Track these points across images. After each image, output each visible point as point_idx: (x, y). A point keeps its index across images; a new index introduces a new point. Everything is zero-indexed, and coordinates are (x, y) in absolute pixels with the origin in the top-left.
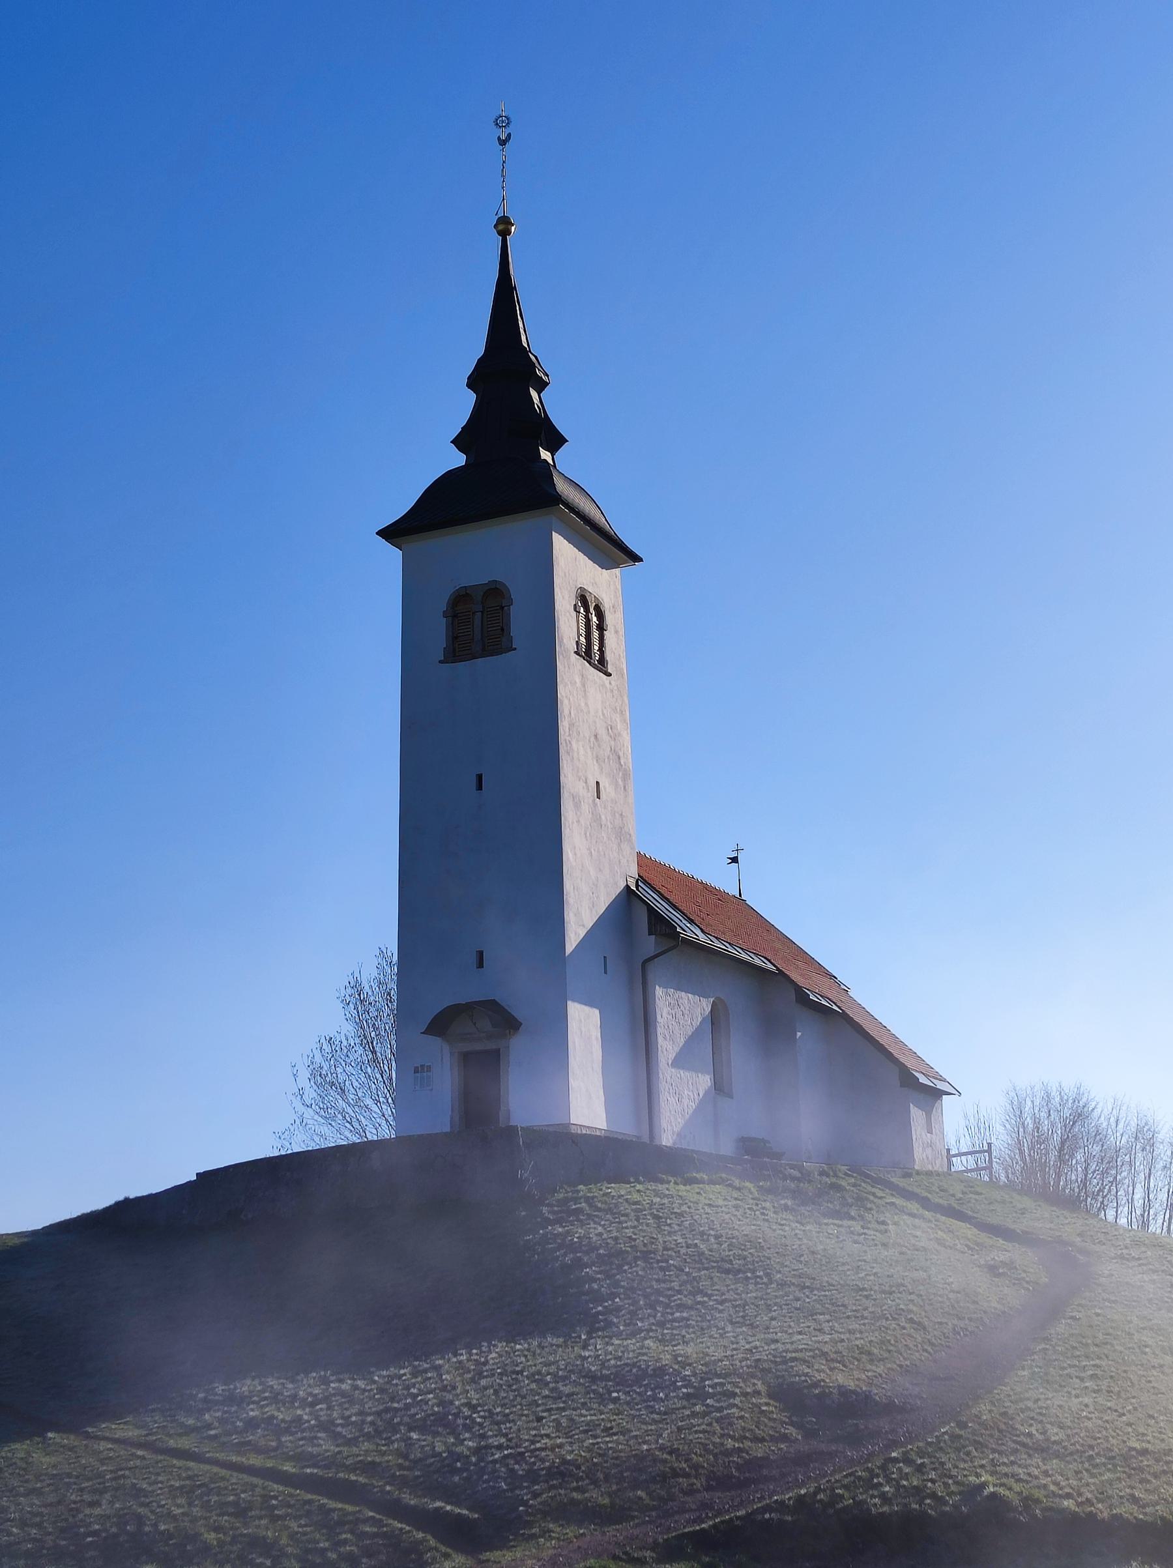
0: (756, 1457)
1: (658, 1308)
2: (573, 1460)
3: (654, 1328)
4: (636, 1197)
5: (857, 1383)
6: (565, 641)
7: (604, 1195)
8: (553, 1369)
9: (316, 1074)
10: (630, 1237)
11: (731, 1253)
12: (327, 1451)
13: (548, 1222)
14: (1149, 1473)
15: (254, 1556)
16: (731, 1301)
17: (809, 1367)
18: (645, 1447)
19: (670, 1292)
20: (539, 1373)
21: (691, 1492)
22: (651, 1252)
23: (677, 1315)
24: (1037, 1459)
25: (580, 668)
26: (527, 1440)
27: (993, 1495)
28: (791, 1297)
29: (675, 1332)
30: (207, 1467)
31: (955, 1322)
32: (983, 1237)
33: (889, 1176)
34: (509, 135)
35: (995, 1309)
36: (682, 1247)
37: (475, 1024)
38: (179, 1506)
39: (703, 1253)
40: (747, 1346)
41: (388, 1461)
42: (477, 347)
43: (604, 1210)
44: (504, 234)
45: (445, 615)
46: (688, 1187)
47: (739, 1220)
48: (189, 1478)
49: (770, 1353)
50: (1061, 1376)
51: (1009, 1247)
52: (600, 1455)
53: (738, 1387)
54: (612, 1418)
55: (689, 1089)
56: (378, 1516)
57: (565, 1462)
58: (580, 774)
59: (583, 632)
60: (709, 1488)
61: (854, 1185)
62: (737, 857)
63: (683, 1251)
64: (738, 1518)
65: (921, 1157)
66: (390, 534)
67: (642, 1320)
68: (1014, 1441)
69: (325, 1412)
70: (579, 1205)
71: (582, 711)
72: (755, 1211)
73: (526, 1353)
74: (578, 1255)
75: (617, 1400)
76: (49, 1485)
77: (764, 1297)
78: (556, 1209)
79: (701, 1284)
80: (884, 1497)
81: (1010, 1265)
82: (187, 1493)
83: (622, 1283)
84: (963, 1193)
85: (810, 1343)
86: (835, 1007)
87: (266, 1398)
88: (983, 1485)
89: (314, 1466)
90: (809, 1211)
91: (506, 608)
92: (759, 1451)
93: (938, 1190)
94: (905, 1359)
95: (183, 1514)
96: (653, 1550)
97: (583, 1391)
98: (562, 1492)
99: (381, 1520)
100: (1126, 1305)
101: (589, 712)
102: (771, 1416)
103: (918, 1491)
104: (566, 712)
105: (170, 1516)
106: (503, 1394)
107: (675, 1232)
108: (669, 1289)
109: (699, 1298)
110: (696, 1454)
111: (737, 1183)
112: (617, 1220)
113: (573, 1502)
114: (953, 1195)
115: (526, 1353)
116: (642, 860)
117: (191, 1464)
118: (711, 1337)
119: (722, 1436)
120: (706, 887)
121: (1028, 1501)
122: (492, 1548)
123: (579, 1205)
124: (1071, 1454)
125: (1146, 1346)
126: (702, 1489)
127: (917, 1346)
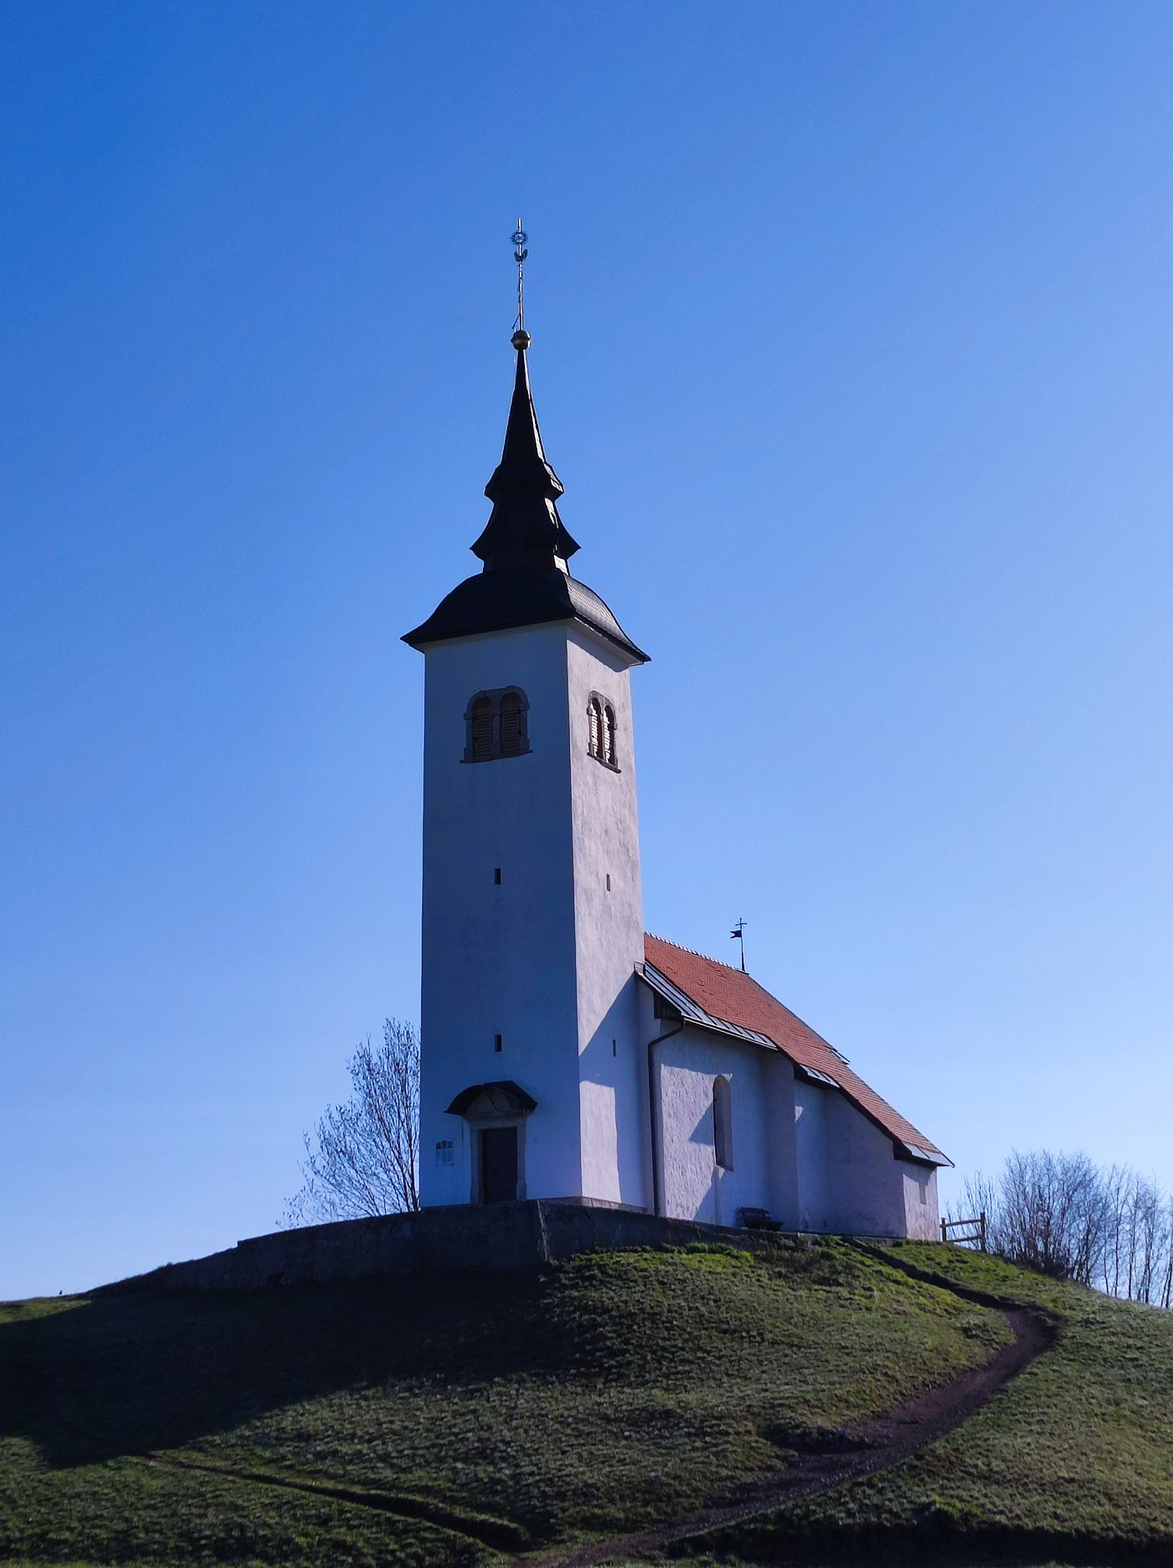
0: (745, 1483)
1: (664, 1363)
2: (593, 1484)
3: (660, 1379)
4: (643, 1265)
5: (834, 1425)
6: (578, 744)
7: (614, 1263)
8: (573, 1412)
9: (326, 1142)
10: (638, 1301)
11: (729, 1315)
12: (386, 1477)
13: (565, 1287)
14: (1072, 1496)
15: (338, 1554)
16: (727, 1357)
17: (793, 1411)
18: (653, 1474)
19: (674, 1350)
20: (562, 1416)
21: (692, 1509)
22: (656, 1314)
23: (680, 1368)
24: (980, 1484)
25: (592, 768)
26: (555, 1469)
27: (939, 1511)
28: (781, 1354)
29: (678, 1383)
30: (289, 1489)
31: (926, 1376)
32: (962, 1303)
33: (880, 1246)
34: (526, 252)
35: (963, 1365)
36: (685, 1310)
37: (494, 1103)
38: (271, 1518)
39: (703, 1315)
40: (740, 1395)
41: (439, 1485)
42: (495, 458)
43: (615, 1277)
45: (466, 716)
46: (690, 1256)
47: (737, 1286)
48: (275, 1497)
49: (760, 1400)
50: (1011, 1421)
51: (984, 1311)
52: (616, 1480)
53: (731, 1427)
54: (625, 1452)
55: (691, 1163)
56: (435, 1526)
57: (587, 1485)
58: (592, 869)
59: (595, 733)
60: (706, 1506)
61: (845, 1254)
62: (740, 931)
63: (686, 1313)
64: (729, 1527)
65: (915, 1227)
66: (414, 639)
67: (649, 1372)
68: (962, 1471)
69: (381, 1447)
70: (592, 1272)
71: (593, 808)
72: (751, 1278)
73: (550, 1400)
74: (592, 1316)
75: (627, 1438)
76: (160, 1502)
77: (757, 1353)
78: (571, 1275)
79: (701, 1342)
80: (850, 1514)
81: (984, 1328)
82: (277, 1508)
83: (632, 1341)
84: (950, 1261)
85: (795, 1392)
86: (833, 1083)
87: (329, 1436)
88: (934, 1502)
89: (378, 1488)
90: (800, 1278)
91: (523, 713)
92: (748, 1478)
93: (925, 1259)
94: (878, 1406)
95: (277, 1523)
96: (660, 1550)
97: (600, 1430)
98: (585, 1508)
99: (437, 1529)
100: (1083, 1363)
101: (600, 810)
102: (759, 1451)
103: (878, 1509)
104: (579, 811)
105: (266, 1525)
106: (531, 1433)
107: (678, 1296)
108: (672, 1346)
109: (700, 1354)
110: (695, 1479)
111: (735, 1252)
112: (627, 1285)
113: (594, 1515)
114: (939, 1264)
115: (550, 1400)
116: (650, 942)
117: (275, 1487)
118: (709, 1387)
119: (717, 1466)
120: (709, 963)
121: (967, 1516)
122: (530, 1550)
123: (592, 1272)
124: (1009, 1481)
125: (1093, 1398)
126: (700, 1507)
127: (889, 1396)
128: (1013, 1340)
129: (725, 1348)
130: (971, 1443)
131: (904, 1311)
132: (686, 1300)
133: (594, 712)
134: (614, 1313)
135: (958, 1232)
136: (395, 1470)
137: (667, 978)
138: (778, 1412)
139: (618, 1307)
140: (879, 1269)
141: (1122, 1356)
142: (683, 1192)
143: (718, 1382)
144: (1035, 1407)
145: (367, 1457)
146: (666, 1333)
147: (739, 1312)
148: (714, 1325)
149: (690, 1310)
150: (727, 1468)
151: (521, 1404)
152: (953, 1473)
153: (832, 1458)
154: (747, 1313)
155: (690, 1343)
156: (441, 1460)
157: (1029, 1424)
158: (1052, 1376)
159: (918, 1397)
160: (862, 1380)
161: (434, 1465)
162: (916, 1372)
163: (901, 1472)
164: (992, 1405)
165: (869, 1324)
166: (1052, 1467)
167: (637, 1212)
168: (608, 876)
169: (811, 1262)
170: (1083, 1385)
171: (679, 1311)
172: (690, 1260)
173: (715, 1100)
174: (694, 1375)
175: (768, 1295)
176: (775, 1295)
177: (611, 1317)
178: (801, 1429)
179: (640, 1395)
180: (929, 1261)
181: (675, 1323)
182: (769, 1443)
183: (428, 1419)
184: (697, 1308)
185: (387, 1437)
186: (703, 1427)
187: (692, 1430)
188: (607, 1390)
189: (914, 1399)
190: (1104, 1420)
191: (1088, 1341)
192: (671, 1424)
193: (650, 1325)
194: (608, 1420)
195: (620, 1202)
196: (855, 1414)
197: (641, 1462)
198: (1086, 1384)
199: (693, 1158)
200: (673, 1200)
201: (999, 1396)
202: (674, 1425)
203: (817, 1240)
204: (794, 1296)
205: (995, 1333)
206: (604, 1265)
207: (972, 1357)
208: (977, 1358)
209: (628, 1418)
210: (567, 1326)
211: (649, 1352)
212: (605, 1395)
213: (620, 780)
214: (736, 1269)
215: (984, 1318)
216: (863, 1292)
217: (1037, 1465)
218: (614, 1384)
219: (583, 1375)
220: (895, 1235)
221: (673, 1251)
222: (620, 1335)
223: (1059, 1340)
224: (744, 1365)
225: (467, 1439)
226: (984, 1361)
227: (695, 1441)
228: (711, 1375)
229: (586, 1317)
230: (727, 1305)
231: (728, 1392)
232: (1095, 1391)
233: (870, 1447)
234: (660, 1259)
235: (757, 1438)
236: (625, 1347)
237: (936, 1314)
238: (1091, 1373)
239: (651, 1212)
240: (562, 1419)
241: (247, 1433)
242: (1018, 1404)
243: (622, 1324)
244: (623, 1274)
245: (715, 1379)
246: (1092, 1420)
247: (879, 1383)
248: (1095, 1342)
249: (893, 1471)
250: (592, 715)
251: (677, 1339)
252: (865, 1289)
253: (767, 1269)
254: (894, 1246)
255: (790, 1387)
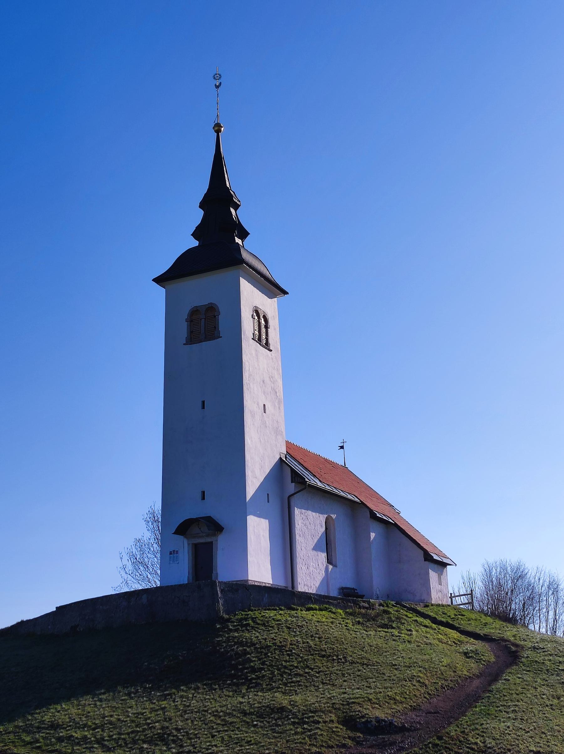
1: (285, 676)
3: (281, 686)
4: (279, 617)
5: (386, 715)
8: (224, 709)
9: (132, 556)
10: (273, 638)
11: (326, 646)
13: (231, 630)
16: (323, 672)
17: (361, 707)
19: (292, 668)
20: (217, 711)
22: (283, 646)
31: (443, 682)
32: (463, 638)
34: (220, 83)
35: (465, 675)
39: (311, 647)
40: (329, 696)
43: (261, 624)
44: (218, 132)
46: (307, 612)
47: (333, 629)
50: (496, 711)
61: (397, 611)
62: (343, 446)
65: (436, 597)
66: (159, 280)
67: (275, 682)
68: (467, 747)
70: (247, 622)
71: (256, 368)
73: (211, 700)
74: (244, 648)
79: (309, 663)
81: (476, 652)
83: (266, 663)
84: (455, 615)
85: (363, 694)
86: (390, 521)
87: (70, 726)
90: (370, 624)
91: (216, 317)
93: (442, 614)
101: (260, 369)
102: (338, 734)
107: (297, 635)
109: (307, 670)
111: (334, 610)
114: (449, 616)
115: (211, 700)
118: (310, 691)
120: (326, 460)
123: (247, 622)
125: (544, 695)
127: (420, 695)
128: (493, 659)
129: (323, 667)
130: (473, 727)
131: (430, 643)
132: (302, 637)
133: (256, 318)
134: (257, 646)
135: (457, 601)
136: (104, 750)
137: (300, 463)
138: (351, 707)
139: (260, 642)
140: (416, 619)
141: (557, 668)
142: (308, 578)
143: (317, 688)
144: (509, 701)
145: (89, 740)
146: (288, 658)
147: (332, 645)
148: (317, 652)
149: (303, 643)
150: (316, 746)
151: (193, 703)
152: (461, 749)
153: (384, 738)
154: (337, 645)
155: (302, 664)
156: (134, 742)
157: (508, 713)
158: (518, 681)
159: (438, 696)
160: (404, 685)
161: (129, 746)
162: (437, 679)
163: (428, 749)
164: (484, 701)
165: (410, 651)
166: (524, 743)
167: (283, 588)
168: (264, 405)
169: (378, 615)
170: (537, 687)
171: (297, 644)
172: (307, 614)
173: (326, 529)
174: (302, 684)
175: (351, 634)
176: (355, 634)
177: (256, 648)
178: (365, 719)
179: (268, 697)
180: (444, 615)
181: (294, 651)
182: (345, 728)
183: (134, 714)
184: (308, 642)
185: (106, 726)
186: (303, 718)
187: (297, 720)
188: (248, 694)
189: (436, 697)
190: (552, 709)
191: (537, 659)
192: (284, 716)
193: (278, 653)
194: (245, 713)
195: (272, 583)
196: (400, 707)
197: (261, 743)
198: (538, 686)
199: (314, 559)
200: (302, 582)
201: (488, 695)
202: (285, 717)
203: (381, 603)
204: (367, 635)
205: (483, 655)
206: (255, 618)
207: (470, 670)
208: (473, 670)
209: (258, 713)
210: (229, 654)
211: (276, 669)
212: (246, 697)
213: (271, 355)
214: (333, 620)
215: (476, 646)
216: (406, 632)
217: (515, 741)
218: (252, 690)
219: (234, 684)
220: (425, 602)
221: (297, 610)
222: (260, 659)
223: (520, 659)
224: (333, 677)
225: (154, 728)
226: (477, 672)
227: (297, 728)
228: (312, 683)
229: (241, 648)
230: (326, 640)
231: (322, 694)
232: (545, 690)
233: (408, 730)
234: (289, 614)
235: (337, 725)
236: (262, 666)
237: (448, 644)
238: (540, 679)
239: (290, 589)
240: (216, 713)
241: (21, 724)
242: (499, 699)
243: (262, 652)
244: (266, 623)
245: (314, 686)
246: (545, 709)
247: (415, 687)
248: (540, 659)
249: (423, 748)
250: (254, 319)
251: (294, 661)
252: (407, 630)
253: (352, 619)
254: (425, 607)
255: (360, 690)
